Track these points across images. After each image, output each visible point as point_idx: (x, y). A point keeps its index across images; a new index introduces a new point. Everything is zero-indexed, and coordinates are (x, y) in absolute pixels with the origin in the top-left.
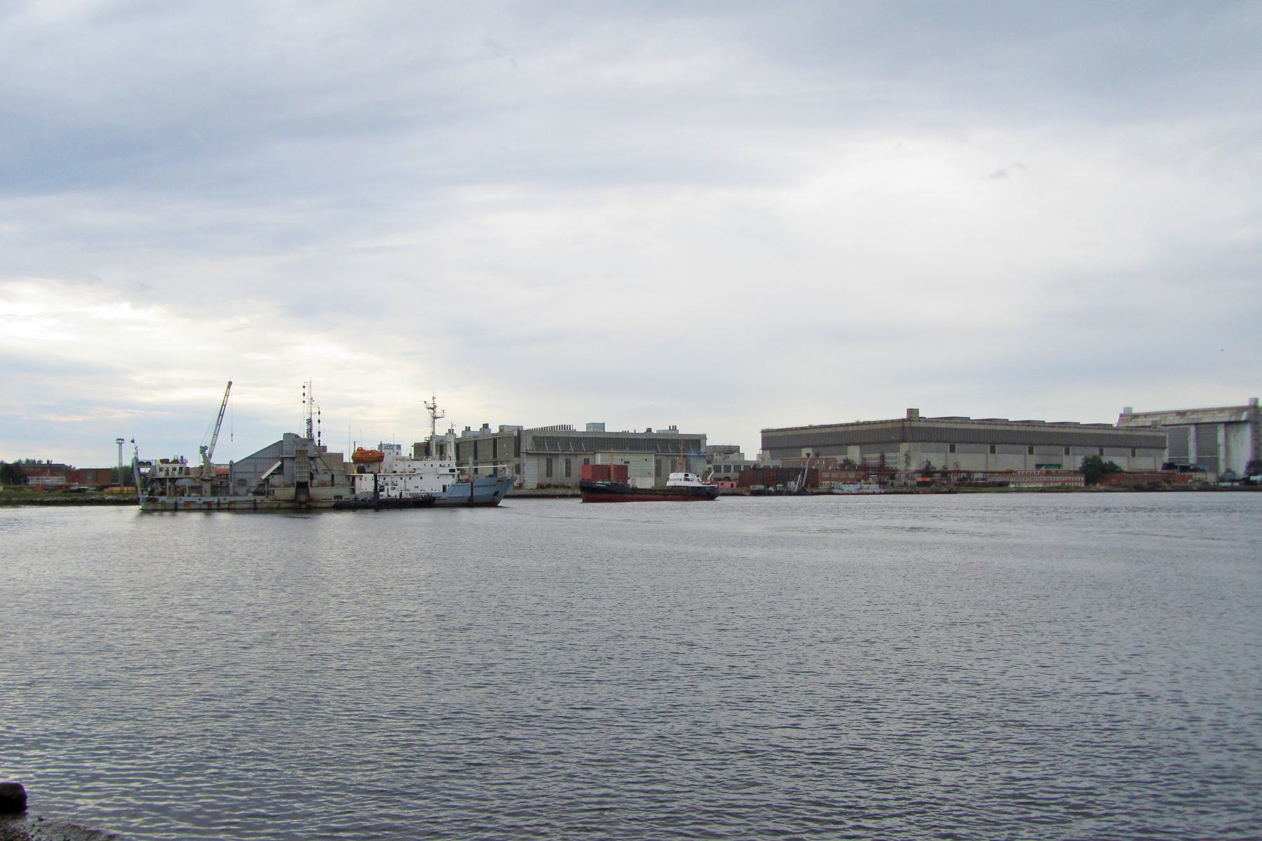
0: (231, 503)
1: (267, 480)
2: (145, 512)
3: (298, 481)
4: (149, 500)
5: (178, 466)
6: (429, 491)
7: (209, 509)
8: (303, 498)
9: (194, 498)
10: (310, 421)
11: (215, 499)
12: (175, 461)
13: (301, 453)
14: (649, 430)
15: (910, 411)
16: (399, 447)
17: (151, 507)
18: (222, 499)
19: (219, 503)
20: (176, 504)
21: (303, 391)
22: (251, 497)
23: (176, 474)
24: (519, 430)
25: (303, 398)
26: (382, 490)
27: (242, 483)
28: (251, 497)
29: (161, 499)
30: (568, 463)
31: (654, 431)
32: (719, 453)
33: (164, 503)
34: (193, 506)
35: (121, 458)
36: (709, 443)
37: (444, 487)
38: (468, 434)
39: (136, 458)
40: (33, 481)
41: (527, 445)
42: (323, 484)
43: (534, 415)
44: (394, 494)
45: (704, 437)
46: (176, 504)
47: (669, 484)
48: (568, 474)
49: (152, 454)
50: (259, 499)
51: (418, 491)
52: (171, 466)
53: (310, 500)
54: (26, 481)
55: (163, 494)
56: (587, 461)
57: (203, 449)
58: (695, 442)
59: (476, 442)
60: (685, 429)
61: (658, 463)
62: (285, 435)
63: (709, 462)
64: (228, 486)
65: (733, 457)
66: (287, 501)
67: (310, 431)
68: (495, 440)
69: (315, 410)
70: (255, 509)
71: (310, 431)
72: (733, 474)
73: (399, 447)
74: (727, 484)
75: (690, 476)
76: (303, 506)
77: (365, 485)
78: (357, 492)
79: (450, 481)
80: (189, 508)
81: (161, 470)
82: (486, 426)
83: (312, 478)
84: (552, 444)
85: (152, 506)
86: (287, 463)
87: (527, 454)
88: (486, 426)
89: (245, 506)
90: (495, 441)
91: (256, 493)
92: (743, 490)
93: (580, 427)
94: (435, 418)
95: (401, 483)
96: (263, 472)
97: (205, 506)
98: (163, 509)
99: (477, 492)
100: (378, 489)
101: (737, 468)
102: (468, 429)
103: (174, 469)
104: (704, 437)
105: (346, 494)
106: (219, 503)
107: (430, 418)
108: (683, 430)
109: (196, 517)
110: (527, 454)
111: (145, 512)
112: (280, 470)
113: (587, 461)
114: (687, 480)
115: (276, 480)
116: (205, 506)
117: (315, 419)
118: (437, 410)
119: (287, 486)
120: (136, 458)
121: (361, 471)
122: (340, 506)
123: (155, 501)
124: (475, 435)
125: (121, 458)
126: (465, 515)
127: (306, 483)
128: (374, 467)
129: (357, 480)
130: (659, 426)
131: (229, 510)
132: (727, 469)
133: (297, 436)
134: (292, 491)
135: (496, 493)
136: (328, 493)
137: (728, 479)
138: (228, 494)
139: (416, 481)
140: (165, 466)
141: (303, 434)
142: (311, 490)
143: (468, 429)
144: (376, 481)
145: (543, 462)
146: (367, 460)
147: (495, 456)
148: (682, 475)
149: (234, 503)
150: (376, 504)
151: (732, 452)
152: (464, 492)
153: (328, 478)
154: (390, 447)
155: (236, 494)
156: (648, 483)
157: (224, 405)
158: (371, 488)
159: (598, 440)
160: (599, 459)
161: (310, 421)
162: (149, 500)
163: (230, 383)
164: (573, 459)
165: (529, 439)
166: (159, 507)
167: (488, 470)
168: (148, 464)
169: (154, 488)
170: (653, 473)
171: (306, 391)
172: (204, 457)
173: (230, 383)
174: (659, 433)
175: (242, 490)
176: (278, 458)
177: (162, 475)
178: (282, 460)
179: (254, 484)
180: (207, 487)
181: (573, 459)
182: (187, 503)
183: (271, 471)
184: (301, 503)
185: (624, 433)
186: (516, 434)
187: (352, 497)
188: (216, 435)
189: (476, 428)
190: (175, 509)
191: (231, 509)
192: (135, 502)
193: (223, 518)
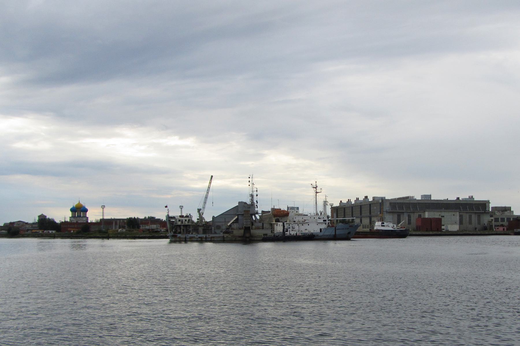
0: (212, 238)
1: (230, 226)
2: (171, 242)
3: (246, 226)
4: (173, 236)
5: (187, 219)
6: (312, 231)
7: (201, 241)
8: (247, 235)
9: (194, 235)
10: (252, 196)
11: (204, 236)
12: (187, 216)
13: (247, 212)
14: (458, 198)
15: (73, 210)
16: (298, 208)
17: (173, 239)
18: (207, 235)
19: (206, 238)
20: (186, 238)
21: (248, 180)
22: (222, 234)
23: (186, 223)
24: (383, 199)
25: (248, 184)
26: (287, 231)
27: (218, 227)
28: (222, 234)
29: (179, 235)
30: (409, 217)
31: (460, 199)
32: (499, 211)
33: (180, 237)
34: (194, 239)
35: (181, 213)
36: (491, 205)
37: (321, 230)
38: (358, 202)
39: (168, 215)
40: (142, 227)
41: (387, 207)
42: (258, 228)
43: (391, 191)
44: (293, 233)
45: (488, 202)
46: (186, 238)
47: (375, 228)
48: (409, 223)
49: (175, 213)
50: (226, 235)
51: (307, 232)
52: (184, 219)
53: (251, 236)
54: (139, 227)
55: (180, 233)
56: (420, 216)
57: (199, 210)
58: (484, 205)
59: (361, 206)
60: (478, 197)
61: (461, 217)
62: (239, 203)
63: (491, 216)
64: (211, 229)
65: (507, 213)
66: (240, 237)
67: (252, 200)
68: (370, 204)
69: (255, 189)
70: (223, 241)
71: (252, 200)
72: (506, 223)
73: (298, 208)
74: (501, 229)
75: (385, 224)
76: (248, 239)
77: (279, 228)
78: (275, 232)
79: (324, 226)
80: (192, 240)
81: (179, 220)
82: (366, 197)
83: (252, 225)
84: (402, 207)
85: (175, 240)
86: (240, 218)
87: (387, 212)
88: (366, 197)
89: (219, 239)
90: (370, 205)
91: (224, 233)
92: (510, 232)
93: (419, 198)
94: (317, 193)
95: (296, 227)
96: (229, 222)
97: (199, 239)
98: (180, 241)
99: (338, 232)
100: (285, 230)
101: (508, 219)
102: (358, 199)
103: (186, 220)
104: (488, 202)
105: (269, 232)
106: (206, 238)
107: (314, 194)
108: (476, 198)
109: (196, 244)
110: (387, 212)
111: (171, 242)
112: (237, 221)
113: (420, 216)
114: (383, 226)
115: (235, 226)
116: (199, 239)
117: (255, 194)
118: (317, 188)
119: (240, 229)
120: (168, 215)
121: (277, 221)
122: (266, 239)
123: (176, 236)
124: (361, 202)
125: (181, 213)
126: (331, 244)
127: (249, 227)
128: (283, 220)
129: (275, 226)
130: (464, 196)
131: (211, 241)
132: (503, 220)
133: (245, 203)
134: (242, 231)
135: (349, 233)
136: (260, 233)
137: (502, 226)
138: (211, 233)
139: (306, 226)
140: (181, 219)
141: (249, 202)
142: (252, 231)
143: (358, 199)
144: (284, 226)
145: (396, 216)
146: (279, 215)
147: (370, 213)
148: (380, 223)
149: (214, 237)
150: (284, 238)
151: (506, 211)
152: (331, 232)
153: (260, 225)
154: (293, 208)
155: (215, 233)
156: (455, 228)
157: (209, 188)
158: (281, 231)
159: (428, 204)
160: (427, 215)
161: (252, 196)
162: (173, 236)
163: (212, 176)
164: (412, 215)
165: (388, 204)
166: (178, 239)
167: (349, 222)
168: (174, 218)
169: (179, 230)
170: (458, 222)
171: (250, 180)
172: (200, 214)
173: (212, 176)
174: (463, 200)
175: (217, 231)
176: (235, 215)
177: (179, 223)
178: (238, 215)
179: (224, 227)
180: (201, 229)
181: (412, 215)
182: (191, 238)
183: (232, 221)
184: (247, 237)
185: (444, 200)
186: (380, 201)
187: (273, 235)
188: (205, 203)
189: (361, 198)
190: (186, 241)
191: (212, 240)
192: (166, 237)
193: (209, 245)
